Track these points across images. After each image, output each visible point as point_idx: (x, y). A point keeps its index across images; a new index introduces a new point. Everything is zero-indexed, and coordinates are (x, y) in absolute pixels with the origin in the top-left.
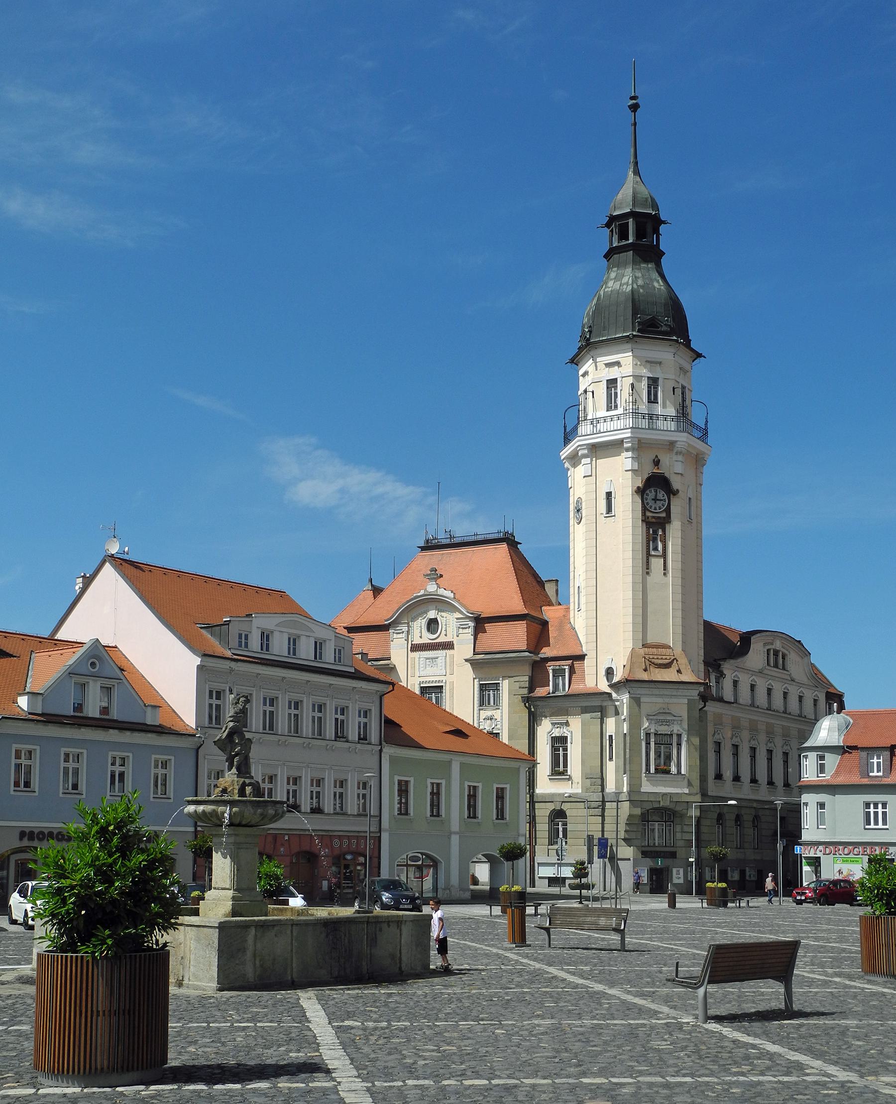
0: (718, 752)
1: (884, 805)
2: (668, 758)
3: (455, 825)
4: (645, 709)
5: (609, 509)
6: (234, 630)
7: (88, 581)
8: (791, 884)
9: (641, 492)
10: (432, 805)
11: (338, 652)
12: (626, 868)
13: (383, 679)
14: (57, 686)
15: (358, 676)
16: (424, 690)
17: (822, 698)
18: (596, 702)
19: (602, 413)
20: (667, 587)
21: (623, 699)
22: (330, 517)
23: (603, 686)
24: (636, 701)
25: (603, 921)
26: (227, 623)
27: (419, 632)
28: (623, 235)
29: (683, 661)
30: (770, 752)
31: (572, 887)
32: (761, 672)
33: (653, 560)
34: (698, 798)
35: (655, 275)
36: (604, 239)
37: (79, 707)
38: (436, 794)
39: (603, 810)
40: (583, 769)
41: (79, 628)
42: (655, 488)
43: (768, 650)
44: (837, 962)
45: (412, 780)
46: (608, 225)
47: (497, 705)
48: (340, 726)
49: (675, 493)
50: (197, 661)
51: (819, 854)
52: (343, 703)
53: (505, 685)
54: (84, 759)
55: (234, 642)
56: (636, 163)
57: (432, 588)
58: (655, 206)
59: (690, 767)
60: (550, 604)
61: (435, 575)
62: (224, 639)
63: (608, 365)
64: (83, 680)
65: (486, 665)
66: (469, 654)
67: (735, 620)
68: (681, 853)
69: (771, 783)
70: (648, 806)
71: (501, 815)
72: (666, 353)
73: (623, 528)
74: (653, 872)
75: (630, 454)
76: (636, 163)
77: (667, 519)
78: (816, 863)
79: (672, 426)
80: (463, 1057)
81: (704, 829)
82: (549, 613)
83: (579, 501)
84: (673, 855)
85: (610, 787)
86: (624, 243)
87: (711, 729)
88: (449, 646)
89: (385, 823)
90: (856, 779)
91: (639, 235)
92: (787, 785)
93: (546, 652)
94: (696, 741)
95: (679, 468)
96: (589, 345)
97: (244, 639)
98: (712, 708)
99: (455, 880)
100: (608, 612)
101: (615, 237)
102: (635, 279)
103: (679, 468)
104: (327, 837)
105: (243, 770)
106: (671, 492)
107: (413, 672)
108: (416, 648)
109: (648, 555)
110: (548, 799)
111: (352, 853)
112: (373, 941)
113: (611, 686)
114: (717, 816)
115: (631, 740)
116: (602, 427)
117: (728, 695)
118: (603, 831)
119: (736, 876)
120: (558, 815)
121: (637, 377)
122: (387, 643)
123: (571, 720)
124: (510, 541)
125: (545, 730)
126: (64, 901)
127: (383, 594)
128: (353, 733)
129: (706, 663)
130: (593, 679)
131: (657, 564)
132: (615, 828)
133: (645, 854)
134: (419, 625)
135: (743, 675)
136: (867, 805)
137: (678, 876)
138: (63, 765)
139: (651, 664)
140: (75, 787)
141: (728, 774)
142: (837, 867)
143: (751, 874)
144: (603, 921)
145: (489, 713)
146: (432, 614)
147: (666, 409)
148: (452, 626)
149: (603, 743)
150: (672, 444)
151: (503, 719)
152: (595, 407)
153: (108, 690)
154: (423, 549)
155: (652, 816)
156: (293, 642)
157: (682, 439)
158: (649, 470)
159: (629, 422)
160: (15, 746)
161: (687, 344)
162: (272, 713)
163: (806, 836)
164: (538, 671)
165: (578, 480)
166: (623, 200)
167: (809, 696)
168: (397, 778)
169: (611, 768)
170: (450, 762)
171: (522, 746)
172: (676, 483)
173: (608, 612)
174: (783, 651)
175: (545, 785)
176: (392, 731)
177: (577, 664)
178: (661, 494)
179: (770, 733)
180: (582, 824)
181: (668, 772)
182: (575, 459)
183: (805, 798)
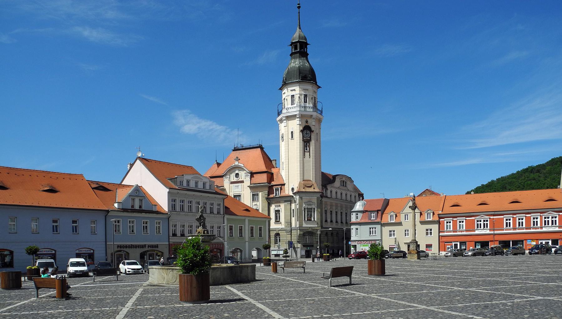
0: (326, 213)
1: (375, 228)
2: (311, 215)
3: (247, 239)
4: (304, 200)
5: (292, 137)
6: (178, 180)
7: (132, 165)
8: (348, 254)
9: (302, 131)
11: (210, 186)
12: (299, 250)
13: (221, 193)
14: (126, 200)
15: (216, 193)
16: (235, 196)
17: (357, 195)
18: (289, 199)
19: (290, 106)
20: (310, 161)
21: (297, 198)
22: (200, 137)
23: (291, 194)
24: (301, 198)
25: (299, 265)
27: (233, 178)
28: (296, 48)
29: (315, 185)
30: (341, 213)
31: (284, 257)
33: (306, 153)
34: (320, 228)
35: (306, 61)
36: (290, 50)
37: (133, 206)
38: (241, 230)
40: (285, 220)
41: (132, 180)
42: (306, 130)
44: (362, 273)
46: (291, 45)
47: (258, 200)
48: (211, 209)
49: (313, 131)
50: (168, 190)
52: (212, 202)
53: (260, 194)
54: (135, 222)
55: (179, 184)
56: (300, 25)
57: (237, 163)
58: (306, 39)
59: (318, 219)
60: (274, 168)
61: (238, 159)
62: (175, 183)
63: (291, 90)
64: (133, 197)
65: (254, 188)
66: (249, 184)
67: (331, 171)
68: (315, 245)
69: (342, 222)
70: (305, 231)
71: (260, 235)
73: (297, 143)
74: (306, 251)
76: (300, 25)
77: (310, 140)
78: (355, 247)
79: (311, 110)
80: (276, 296)
81: (322, 238)
82: (274, 171)
83: (283, 134)
84: (313, 246)
85: (293, 225)
86: (296, 51)
87: (324, 206)
88: (242, 182)
90: (367, 221)
91: (300, 48)
92: (346, 223)
93: (273, 183)
94: (319, 210)
95: (314, 123)
96: (285, 84)
97: (181, 183)
98: (324, 200)
99: (247, 256)
100: (292, 170)
101: (293, 49)
103: (314, 123)
105: (204, 226)
106: (311, 131)
107: (231, 190)
108: (232, 183)
109: (304, 151)
111: (217, 249)
112: (241, 272)
114: (325, 234)
115: (300, 210)
116: (290, 110)
117: (329, 195)
119: (331, 252)
120: (277, 235)
121: (301, 94)
122: (223, 181)
125: (273, 208)
126: (186, 262)
127: (221, 166)
128: (215, 212)
129: (322, 186)
130: (287, 191)
132: (295, 239)
133: (304, 246)
134: (233, 175)
135: (334, 189)
136: (370, 228)
137: (314, 252)
140: (133, 231)
141: (329, 220)
142: (361, 248)
143: (336, 251)
144: (299, 265)
145: (255, 203)
146: (237, 172)
147: (310, 105)
148: (243, 175)
149: (291, 212)
150: (312, 116)
151: (260, 205)
152: (288, 104)
153: (141, 200)
154: (233, 150)
155: (306, 234)
156: (196, 183)
157: (315, 114)
158: (305, 124)
159: (298, 109)
160: (129, 220)
161: (316, 84)
163: (352, 239)
164: (270, 189)
165: (283, 128)
166: (296, 37)
167: (353, 195)
170: (245, 220)
171: (266, 213)
172: (313, 128)
173: (292, 170)
174: (346, 181)
175: (273, 226)
176: (227, 211)
178: (308, 132)
179: (341, 207)
180: (285, 238)
181: (311, 220)
182: (281, 121)
183: (352, 227)
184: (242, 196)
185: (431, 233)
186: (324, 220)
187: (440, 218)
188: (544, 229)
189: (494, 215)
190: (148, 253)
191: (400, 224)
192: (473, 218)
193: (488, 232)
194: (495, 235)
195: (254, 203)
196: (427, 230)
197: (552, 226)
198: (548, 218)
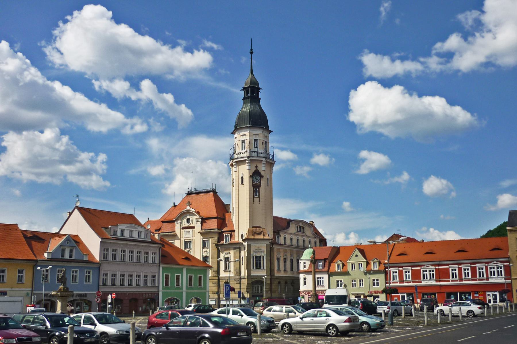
5: (242, 183)
7: (70, 214)
9: (251, 177)
10: (177, 282)
17: (318, 241)
20: (259, 207)
23: (240, 241)
26: (110, 228)
32: (294, 234)
39: (240, 282)
40: (233, 268)
41: (67, 230)
43: (297, 227)
45: (170, 274)
46: (243, 90)
51: (304, 294)
53: (210, 240)
55: (112, 233)
57: (188, 208)
66: (200, 230)
71: (178, 284)
72: (259, 132)
75: (248, 164)
81: (273, 287)
85: (242, 274)
88: (193, 227)
89: (161, 289)
95: (264, 168)
97: (115, 233)
98: (275, 247)
102: (251, 108)
103: (264, 168)
104: (142, 294)
106: (262, 177)
108: (183, 228)
109: (254, 197)
110: (224, 278)
113: (243, 240)
118: (240, 289)
122: (174, 226)
123: (231, 252)
124: (214, 192)
125: (222, 256)
130: (237, 238)
131: (257, 200)
138: (72, 274)
139: (254, 233)
146: (188, 217)
148: (195, 220)
149: (239, 261)
155: (255, 283)
158: (254, 169)
162: (124, 255)
164: (221, 237)
168: (165, 274)
169: (243, 267)
172: (263, 173)
177: (233, 233)
178: (258, 177)
183: (300, 275)
184: (193, 242)
185: (378, 284)
186: (101, 284)
187: (386, 268)
188: (491, 281)
189: (439, 265)
190: (76, 302)
191: (347, 273)
192: (448, 267)
193: (503, 280)
194: (441, 286)
195: (204, 250)
196: (338, 281)
197: (430, 280)
198: (494, 268)
